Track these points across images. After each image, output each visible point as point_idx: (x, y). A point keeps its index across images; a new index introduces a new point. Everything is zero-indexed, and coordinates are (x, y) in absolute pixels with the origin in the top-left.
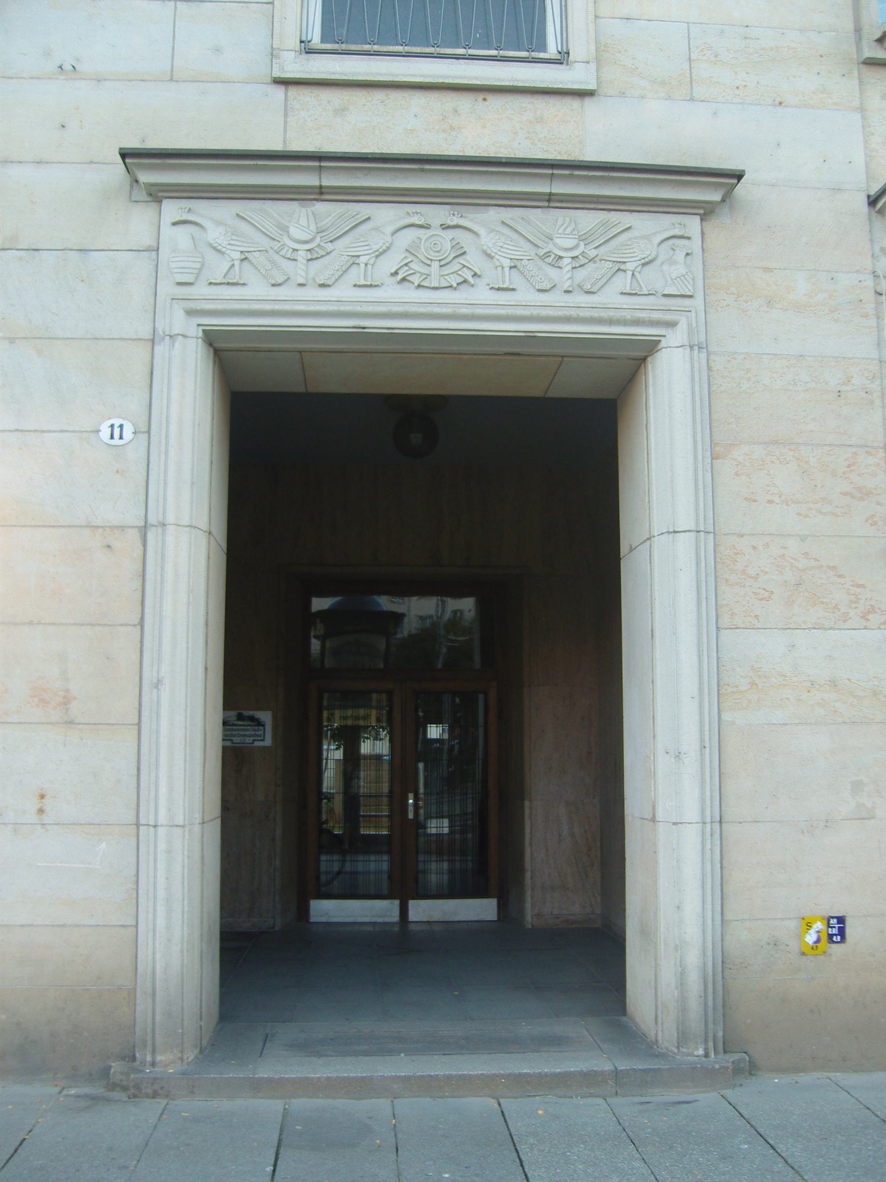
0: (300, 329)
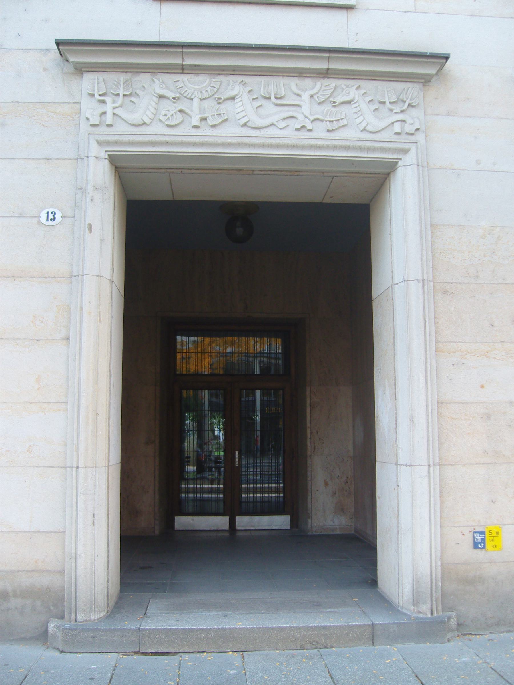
0: (250, 155)
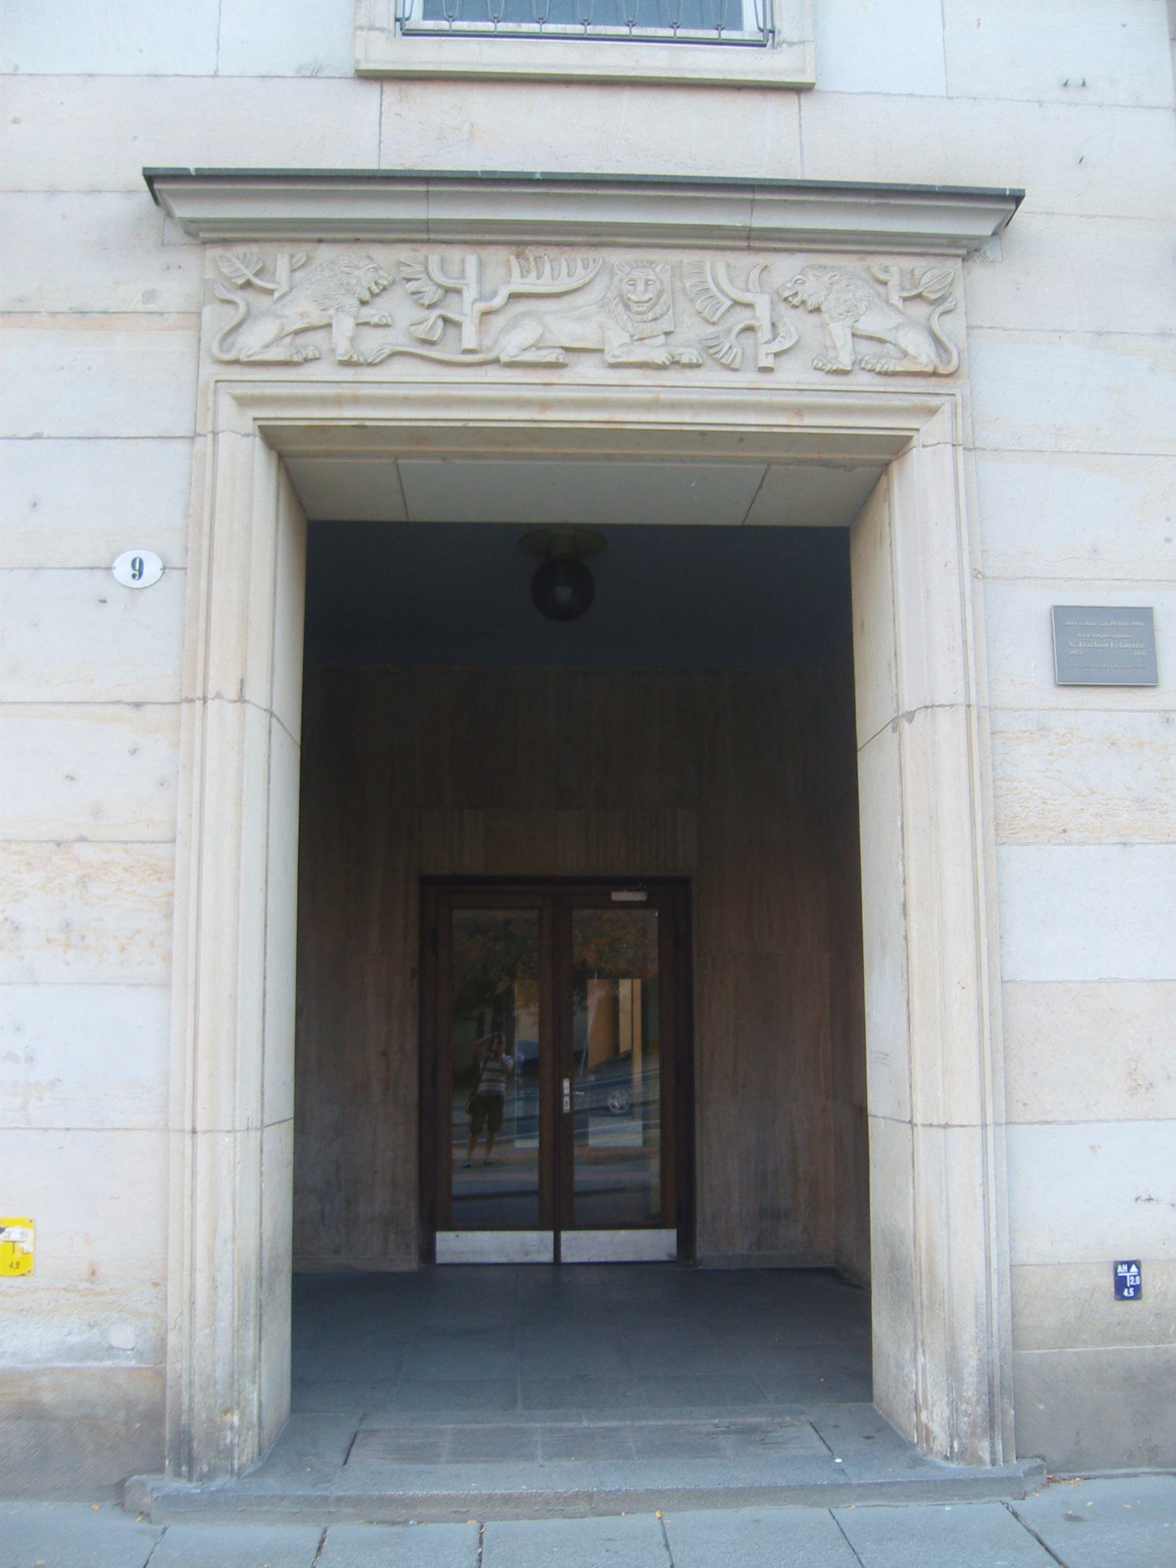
0: (678, 428)
